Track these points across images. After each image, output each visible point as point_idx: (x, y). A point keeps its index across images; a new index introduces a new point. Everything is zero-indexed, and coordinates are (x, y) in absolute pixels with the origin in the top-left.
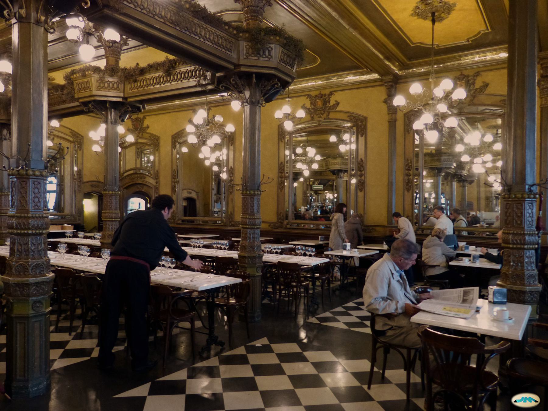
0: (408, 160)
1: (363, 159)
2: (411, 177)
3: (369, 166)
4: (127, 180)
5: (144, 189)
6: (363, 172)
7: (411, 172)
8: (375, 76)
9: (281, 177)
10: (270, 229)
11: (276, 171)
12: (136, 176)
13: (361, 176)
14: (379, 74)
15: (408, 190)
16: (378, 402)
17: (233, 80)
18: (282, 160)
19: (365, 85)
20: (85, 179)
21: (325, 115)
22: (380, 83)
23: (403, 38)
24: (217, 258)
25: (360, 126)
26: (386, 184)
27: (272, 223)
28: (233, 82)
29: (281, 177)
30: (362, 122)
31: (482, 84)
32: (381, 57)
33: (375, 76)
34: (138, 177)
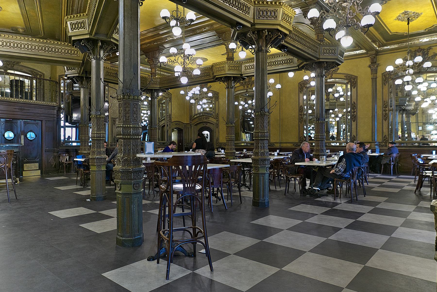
0: (385, 101)
1: (355, 102)
2: (387, 112)
3: (359, 106)
4: (197, 120)
5: (208, 125)
6: (355, 110)
7: (387, 109)
8: (363, 51)
9: (301, 115)
10: (293, 147)
11: (297, 111)
13: (354, 112)
14: (366, 50)
15: (385, 120)
16: (311, 251)
17: (82, 43)
18: (301, 104)
19: (356, 57)
20: (173, 120)
21: (330, 76)
22: (366, 55)
23: (388, 32)
24: (242, 163)
25: (352, 81)
26: (371, 116)
27: (295, 143)
28: (83, 45)
29: (301, 115)
30: (354, 79)
31: (433, 54)
32: (370, 41)
33: (363, 51)
34: (204, 118)
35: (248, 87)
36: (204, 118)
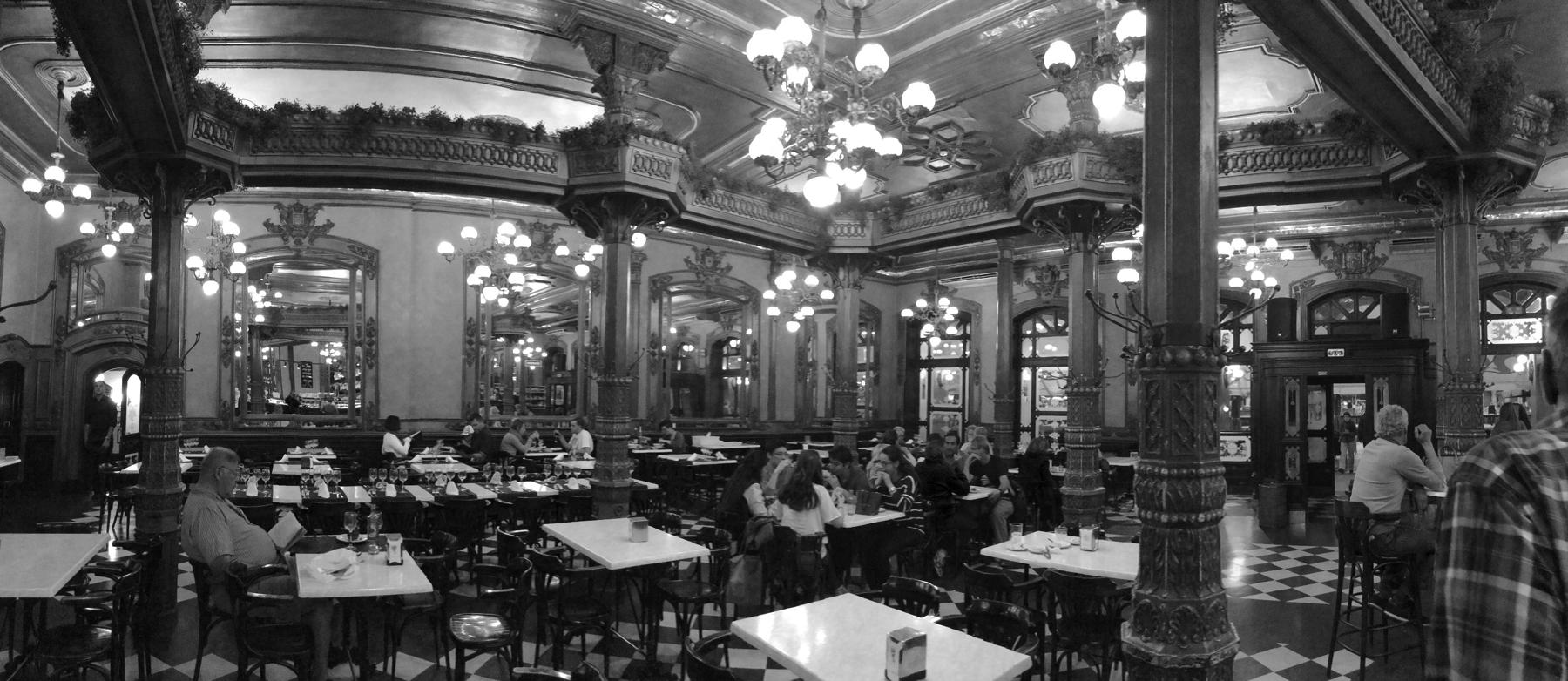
12: (116, 326)
35: (298, 242)
36: (119, 331)
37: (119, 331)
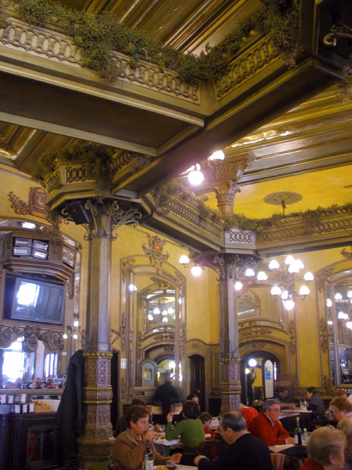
4: (151, 340)
37: (256, 332)
